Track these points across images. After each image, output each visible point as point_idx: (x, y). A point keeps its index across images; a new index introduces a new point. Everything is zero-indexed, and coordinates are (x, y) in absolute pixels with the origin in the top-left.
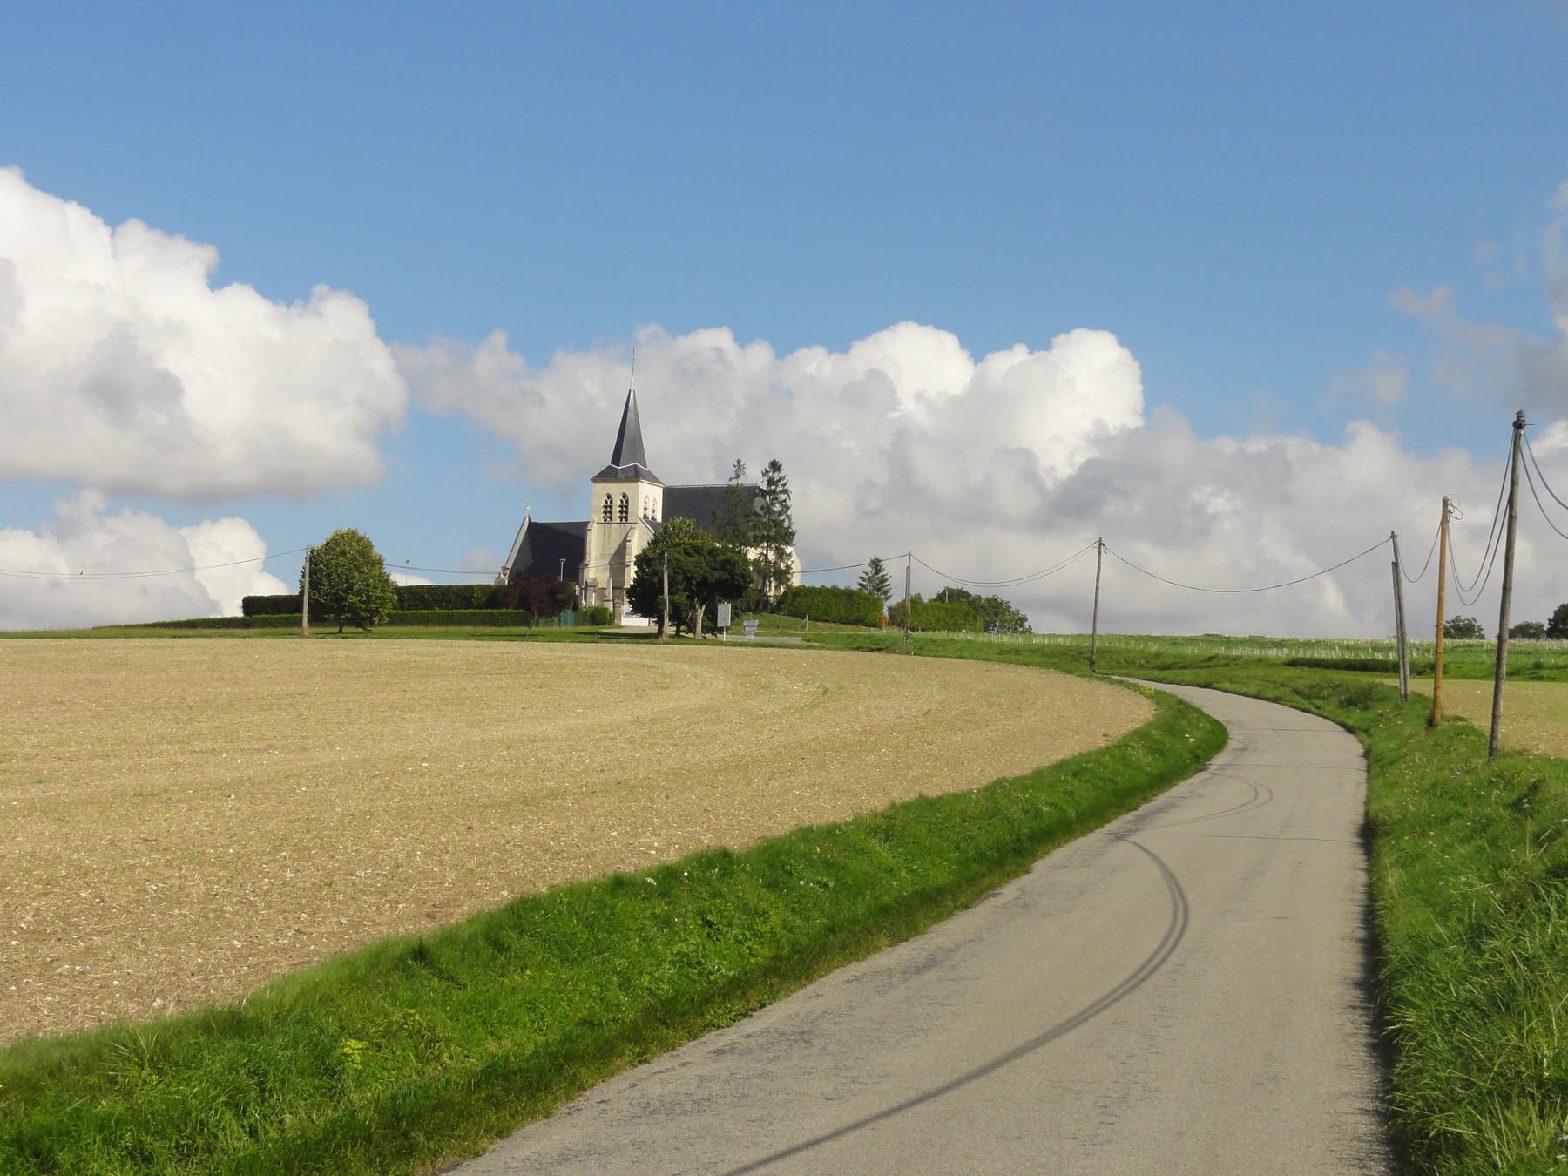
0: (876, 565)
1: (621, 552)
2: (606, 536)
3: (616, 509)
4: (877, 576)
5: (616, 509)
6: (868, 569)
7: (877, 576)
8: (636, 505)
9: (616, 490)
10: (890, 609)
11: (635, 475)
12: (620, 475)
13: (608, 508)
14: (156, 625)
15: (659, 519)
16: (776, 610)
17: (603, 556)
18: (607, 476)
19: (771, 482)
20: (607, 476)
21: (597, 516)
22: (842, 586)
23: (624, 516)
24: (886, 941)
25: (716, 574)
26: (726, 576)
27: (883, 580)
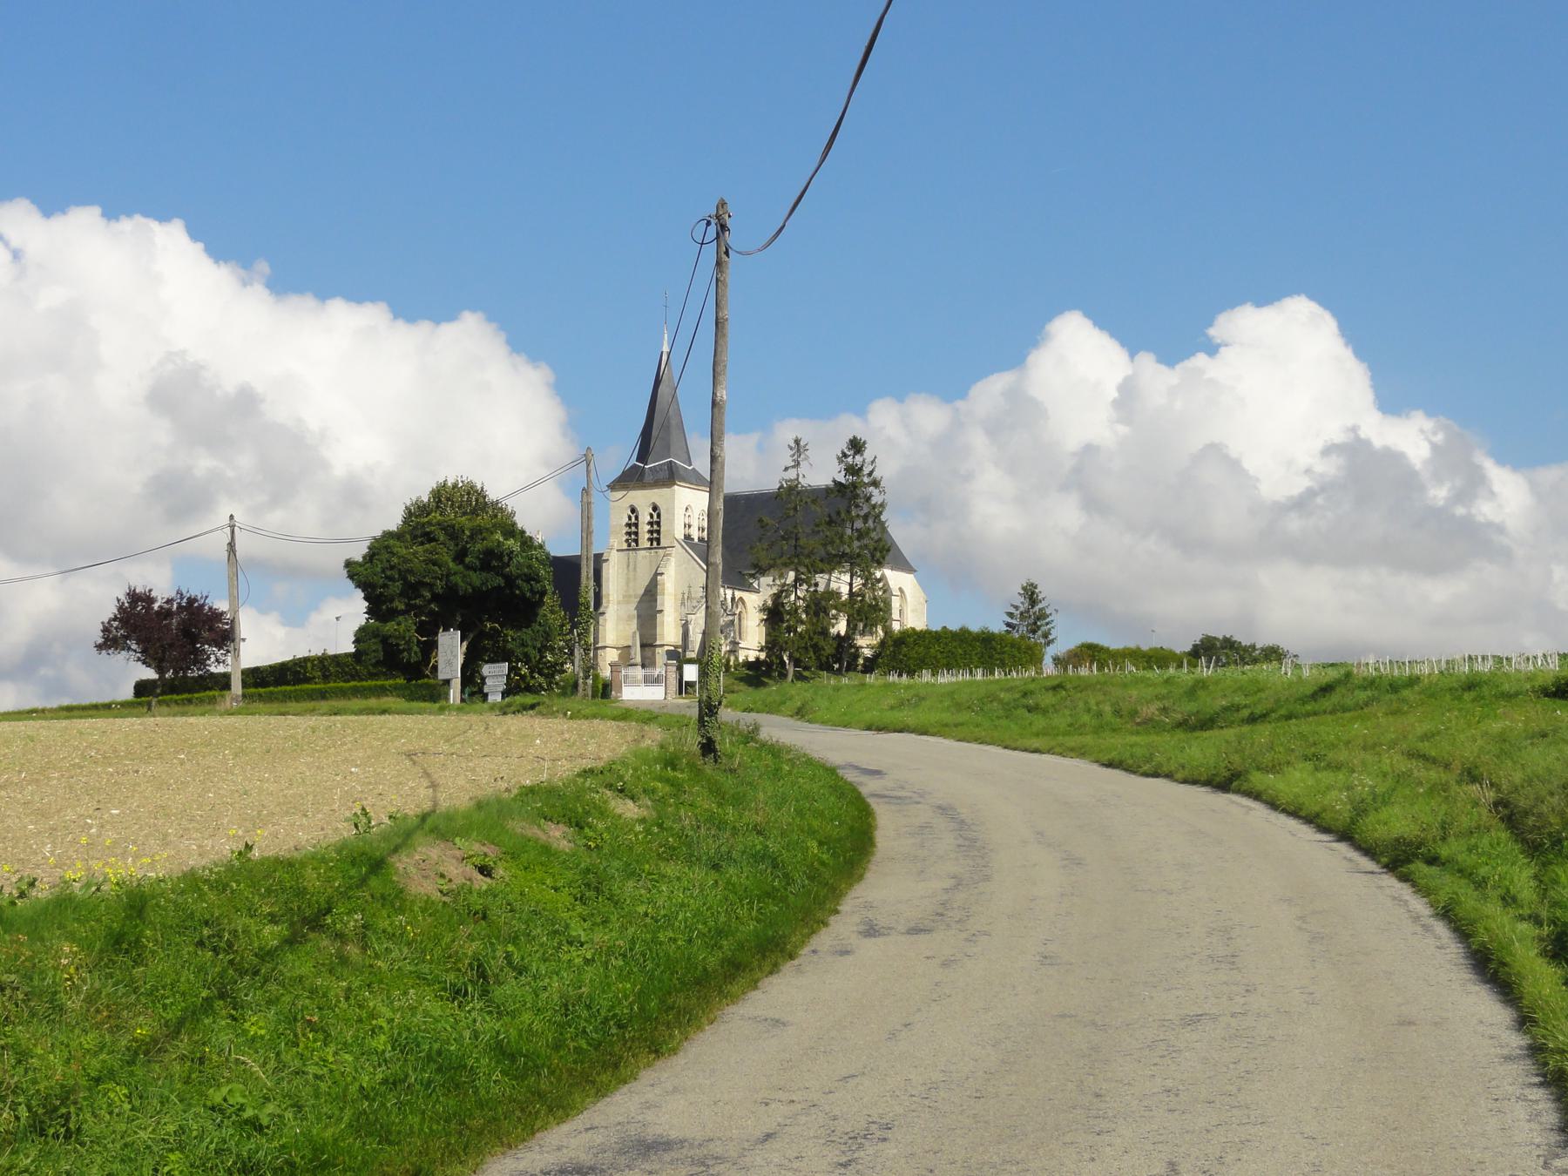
0: (1031, 594)
1: (651, 594)
2: (630, 566)
3: (644, 528)
4: (1033, 610)
5: (644, 528)
6: (1019, 601)
7: (1033, 610)
8: (672, 522)
9: (642, 499)
10: (1057, 660)
11: (670, 477)
12: (648, 478)
13: (633, 525)
14: (95, 707)
16: (870, 666)
17: (627, 598)
18: (630, 479)
19: (853, 470)
20: (630, 479)
21: (619, 540)
22: (975, 627)
24: (1439, 438)
25: (476, 578)
26: (500, 581)
27: (1042, 616)
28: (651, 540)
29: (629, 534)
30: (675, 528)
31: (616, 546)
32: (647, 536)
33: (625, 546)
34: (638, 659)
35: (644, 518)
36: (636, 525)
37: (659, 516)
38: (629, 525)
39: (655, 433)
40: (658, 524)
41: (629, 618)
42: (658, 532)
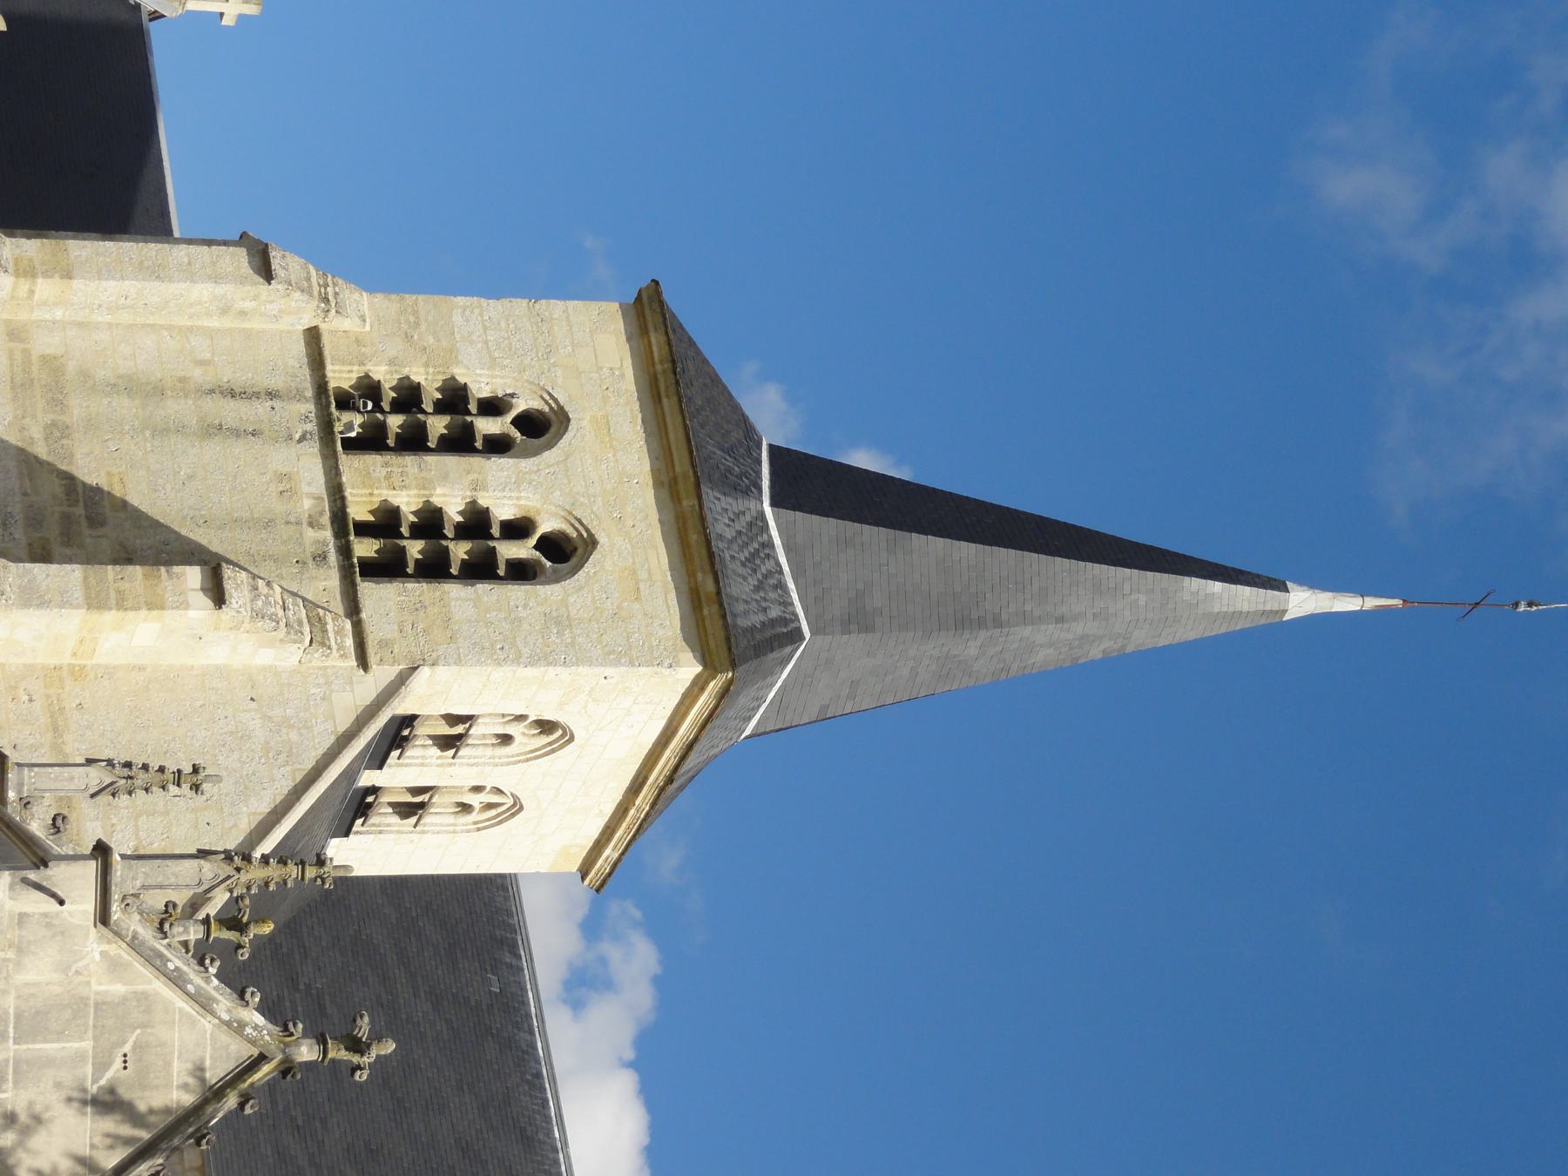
3: (451, 485)
5: (451, 485)
9: (603, 475)
11: (729, 633)
12: (719, 504)
15: (372, 853)
23: (398, 551)
28: (386, 523)
29: (409, 397)
30: (465, 658)
31: (335, 328)
32: (408, 503)
33: (341, 377)
35: (504, 488)
36: (460, 442)
37: (521, 572)
38: (454, 399)
39: (931, 551)
40: (481, 569)
42: (434, 569)
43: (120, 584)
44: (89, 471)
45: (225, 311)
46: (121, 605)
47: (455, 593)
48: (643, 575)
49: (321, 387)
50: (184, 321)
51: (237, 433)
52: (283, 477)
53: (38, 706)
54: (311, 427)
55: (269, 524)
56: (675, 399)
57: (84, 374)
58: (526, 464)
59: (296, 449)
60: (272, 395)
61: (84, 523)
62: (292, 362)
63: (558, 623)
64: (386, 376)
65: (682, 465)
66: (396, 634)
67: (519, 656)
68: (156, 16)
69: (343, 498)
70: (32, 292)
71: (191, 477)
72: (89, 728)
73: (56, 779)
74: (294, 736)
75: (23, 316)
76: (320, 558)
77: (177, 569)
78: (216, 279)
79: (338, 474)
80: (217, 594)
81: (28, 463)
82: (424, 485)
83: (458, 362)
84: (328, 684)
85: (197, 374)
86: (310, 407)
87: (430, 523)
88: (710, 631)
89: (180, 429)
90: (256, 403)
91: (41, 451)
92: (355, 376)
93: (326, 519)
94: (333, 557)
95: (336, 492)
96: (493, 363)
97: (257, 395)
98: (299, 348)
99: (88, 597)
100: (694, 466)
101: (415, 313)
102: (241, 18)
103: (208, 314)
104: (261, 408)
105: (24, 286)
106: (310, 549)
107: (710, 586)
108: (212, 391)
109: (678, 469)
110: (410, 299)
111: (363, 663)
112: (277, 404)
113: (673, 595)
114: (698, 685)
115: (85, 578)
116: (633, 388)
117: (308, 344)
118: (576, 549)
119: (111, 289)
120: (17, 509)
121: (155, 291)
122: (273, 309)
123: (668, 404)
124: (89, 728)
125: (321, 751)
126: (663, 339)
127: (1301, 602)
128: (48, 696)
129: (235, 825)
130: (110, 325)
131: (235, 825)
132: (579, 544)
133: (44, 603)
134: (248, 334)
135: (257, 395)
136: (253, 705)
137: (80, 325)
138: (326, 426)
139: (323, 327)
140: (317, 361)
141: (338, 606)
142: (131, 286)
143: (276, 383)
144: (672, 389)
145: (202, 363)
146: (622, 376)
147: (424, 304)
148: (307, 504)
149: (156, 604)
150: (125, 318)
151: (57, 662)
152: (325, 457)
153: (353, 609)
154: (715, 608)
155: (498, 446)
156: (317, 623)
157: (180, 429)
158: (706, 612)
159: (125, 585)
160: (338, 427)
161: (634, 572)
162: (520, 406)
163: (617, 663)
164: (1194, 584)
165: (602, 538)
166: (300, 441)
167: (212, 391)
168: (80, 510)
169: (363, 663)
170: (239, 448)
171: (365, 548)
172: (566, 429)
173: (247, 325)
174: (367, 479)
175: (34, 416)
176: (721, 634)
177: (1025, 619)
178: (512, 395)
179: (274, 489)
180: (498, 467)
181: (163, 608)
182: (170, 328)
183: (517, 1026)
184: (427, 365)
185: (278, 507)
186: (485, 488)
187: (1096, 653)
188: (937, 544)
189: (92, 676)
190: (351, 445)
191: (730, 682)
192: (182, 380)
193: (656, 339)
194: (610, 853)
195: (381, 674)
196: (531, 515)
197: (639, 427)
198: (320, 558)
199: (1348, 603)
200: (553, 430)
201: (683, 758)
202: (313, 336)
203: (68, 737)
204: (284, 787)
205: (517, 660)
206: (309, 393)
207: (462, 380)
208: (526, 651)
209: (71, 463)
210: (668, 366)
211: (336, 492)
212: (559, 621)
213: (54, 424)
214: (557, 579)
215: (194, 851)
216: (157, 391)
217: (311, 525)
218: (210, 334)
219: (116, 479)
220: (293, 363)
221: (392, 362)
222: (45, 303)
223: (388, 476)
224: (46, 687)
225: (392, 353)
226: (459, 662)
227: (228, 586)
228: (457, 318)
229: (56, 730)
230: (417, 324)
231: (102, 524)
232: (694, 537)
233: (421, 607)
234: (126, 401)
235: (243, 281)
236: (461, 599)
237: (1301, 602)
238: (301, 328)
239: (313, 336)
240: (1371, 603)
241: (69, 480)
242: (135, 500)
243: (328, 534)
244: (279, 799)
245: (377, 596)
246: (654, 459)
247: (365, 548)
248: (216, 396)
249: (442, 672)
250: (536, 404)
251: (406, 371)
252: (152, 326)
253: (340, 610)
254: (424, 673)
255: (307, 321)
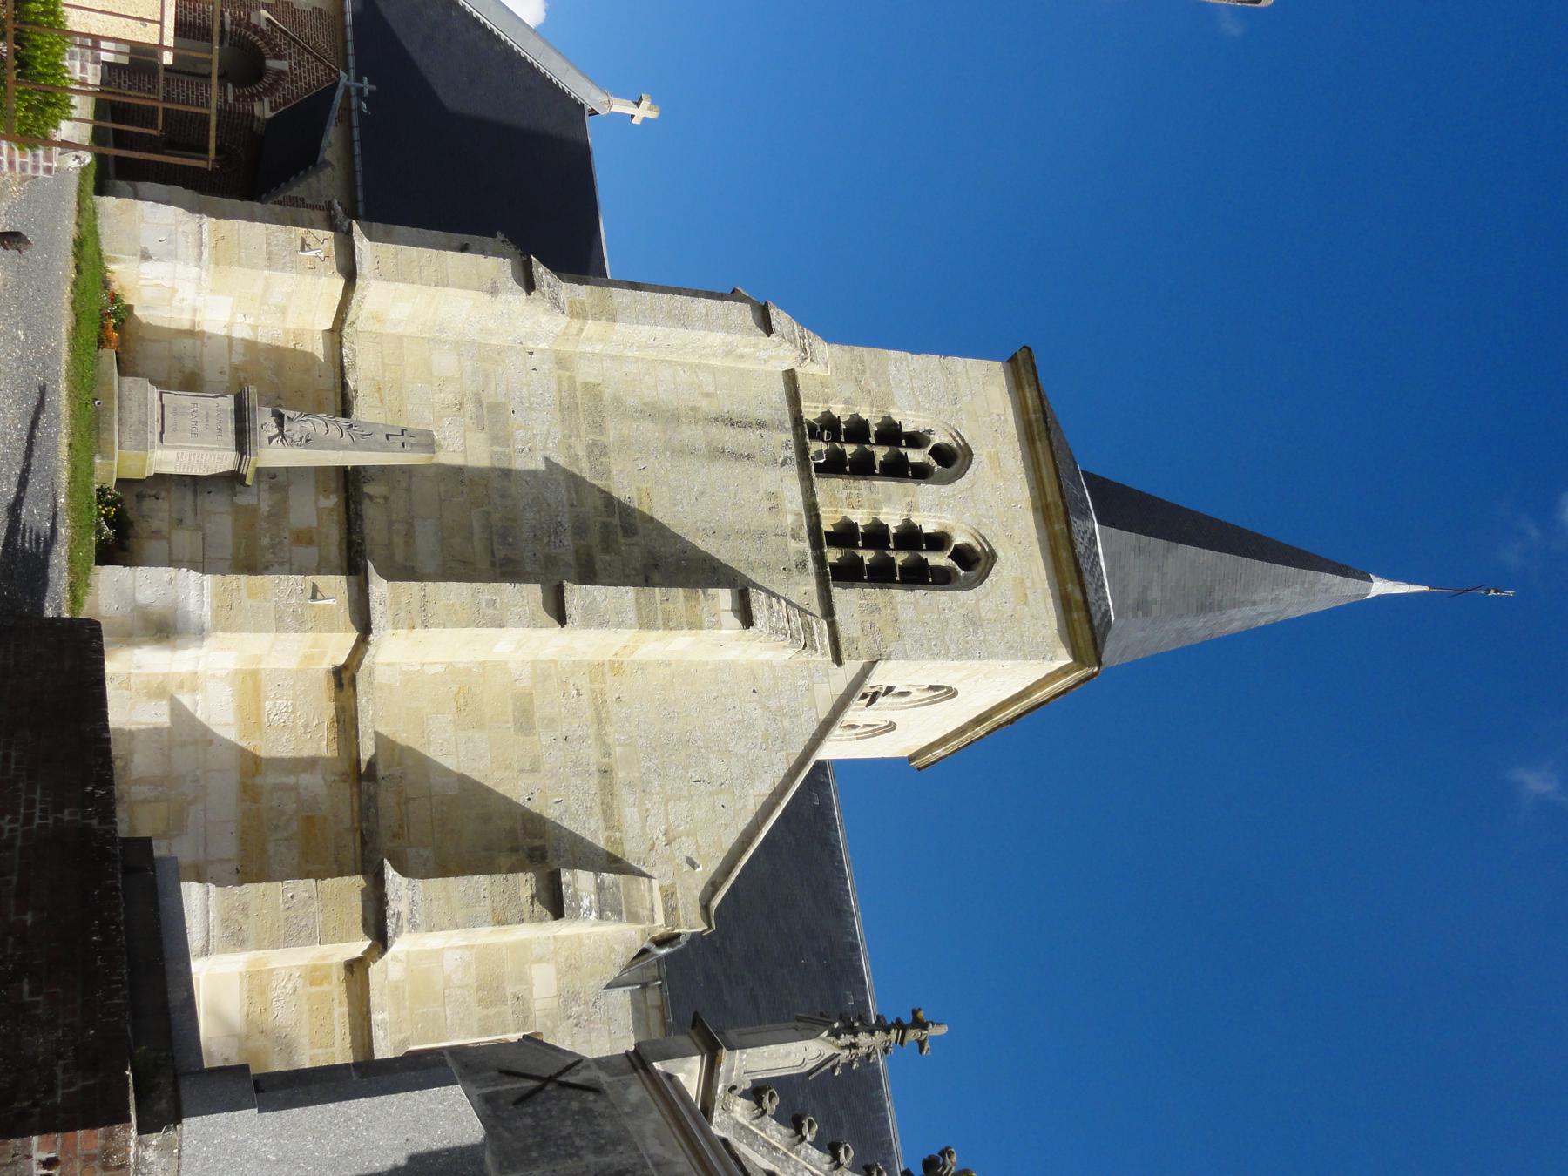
9: (991, 502)
17: (585, 404)
28: (845, 535)
29: (858, 431)
31: (809, 373)
32: (861, 518)
34: (273, 454)
36: (897, 469)
38: (891, 433)
40: (917, 576)
41: (491, 415)
43: (665, 605)
44: (624, 488)
45: (727, 354)
46: (667, 625)
47: (899, 595)
48: (1029, 584)
49: (798, 419)
50: (695, 360)
51: (736, 456)
52: (771, 495)
53: (585, 699)
54: (791, 453)
55: (762, 535)
56: (1046, 443)
57: (618, 401)
58: (945, 490)
59: (780, 471)
60: (761, 425)
61: (620, 533)
62: (774, 398)
63: (974, 624)
64: (840, 411)
65: (1052, 495)
66: (859, 633)
67: (948, 651)
68: (593, 113)
69: (818, 516)
70: (581, 330)
71: (702, 493)
72: (627, 719)
73: (770, 1057)
74: (786, 723)
75: (569, 348)
76: (801, 566)
77: (711, 591)
78: (728, 329)
79: (813, 494)
80: (747, 620)
81: (575, 482)
82: (876, 505)
83: (894, 404)
84: (811, 676)
85: (704, 403)
86: (790, 436)
87: (877, 535)
88: (1079, 631)
89: (693, 451)
90: (749, 431)
91: (585, 470)
92: (819, 411)
93: (804, 532)
94: (811, 565)
95: (812, 509)
96: (918, 406)
97: (749, 424)
98: (780, 386)
99: (639, 617)
100: (1062, 497)
101: (862, 362)
102: (645, 120)
103: (714, 356)
104: (753, 435)
105: (576, 324)
106: (794, 558)
107: (1078, 596)
108: (716, 420)
109: (1050, 498)
110: (858, 350)
111: (838, 660)
112: (764, 432)
113: (1050, 600)
114: (1064, 671)
115: (637, 600)
116: (1014, 431)
117: (786, 383)
118: (978, 560)
119: (645, 332)
120: (566, 519)
121: (678, 335)
122: (764, 355)
123: (1041, 446)
124: (627, 719)
125: (808, 737)
126: (1036, 393)
127: (1380, 587)
128: (593, 691)
129: (744, 807)
130: (637, 359)
131: (744, 807)
132: (982, 556)
133: (603, 624)
134: (741, 372)
135: (749, 424)
136: (755, 696)
137: (613, 357)
138: (803, 452)
139: (798, 370)
140: (794, 399)
141: (816, 608)
142: (661, 331)
143: (764, 415)
144: (1044, 434)
145: (708, 395)
146: (1006, 421)
147: (866, 352)
148: (790, 519)
149: (695, 625)
150: (650, 354)
151: (600, 659)
152: (802, 479)
153: (829, 612)
154: (1083, 614)
155: (921, 473)
156: (807, 627)
157: (693, 451)
158: (1075, 616)
159: (670, 606)
160: (812, 453)
161: (1022, 581)
162: (936, 440)
163: (1015, 657)
164: (1327, 577)
165: (1000, 553)
166: (782, 465)
167: (716, 420)
168: (616, 521)
169: (838, 660)
170: (738, 468)
171: (833, 555)
172: (970, 463)
173: (742, 366)
174: (834, 501)
175: (578, 436)
176: (1088, 636)
177: (1236, 604)
178: (930, 432)
179: (765, 505)
180: (925, 492)
181: (701, 628)
182: (683, 364)
183: (829, 826)
184: (872, 405)
185: (769, 521)
186: (917, 510)
187: (1262, 623)
188: (1193, 550)
189: (628, 672)
190: (820, 469)
191: (1096, 674)
192: (693, 409)
193: (1030, 394)
194: (940, 752)
195: (852, 667)
196: (948, 530)
197: (1020, 463)
198: (801, 566)
199: (1401, 589)
200: (959, 462)
201: (1028, 711)
202: (790, 377)
203: (610, 729)
204: (781, 770)
205: (946, 656)
206: (789, 425)
207: (897, 419)
208: (952, 647)
209: (608, 478)
210: (1039, 415)
211: (812, 509)
212: (973, 621)
213: (594, 443)
214: (969, 585)
215: (340, 282)
216: (672, 418)
217: (794, 537)
218: (713, 370)
219: (644, 494)
220: (775, 398)
221: (847, 401)
222: (589, 339)
223: (848, 498)
224: (591, 681)
225: (847, 394)
226: (906, 657)
227: (754, 608)
228: (892, 369)
229: (599, 721)
230: (864, 371)
231: (635, 533)
232: (1064, 555)
233: (875, 609)
234: (651, 426)
235: (748, 332)
236: (905, 601)
237: (1380, 587)
238: (781, 370)
239: (790, 377)
240: (1414, 588)
241: (609, 500)
242: (658, 516)
243: (806, 545)
244: (778, 781)
245: (848, 600)
246: (1031, 489)
247: (833, 555)
248: (720, 424)
249: (891, 664)
250: (947, 440)
251: (856, 410)
252: (669, 362)
253: (818, 612)
254: (881, 664)
255: (787, 366)
